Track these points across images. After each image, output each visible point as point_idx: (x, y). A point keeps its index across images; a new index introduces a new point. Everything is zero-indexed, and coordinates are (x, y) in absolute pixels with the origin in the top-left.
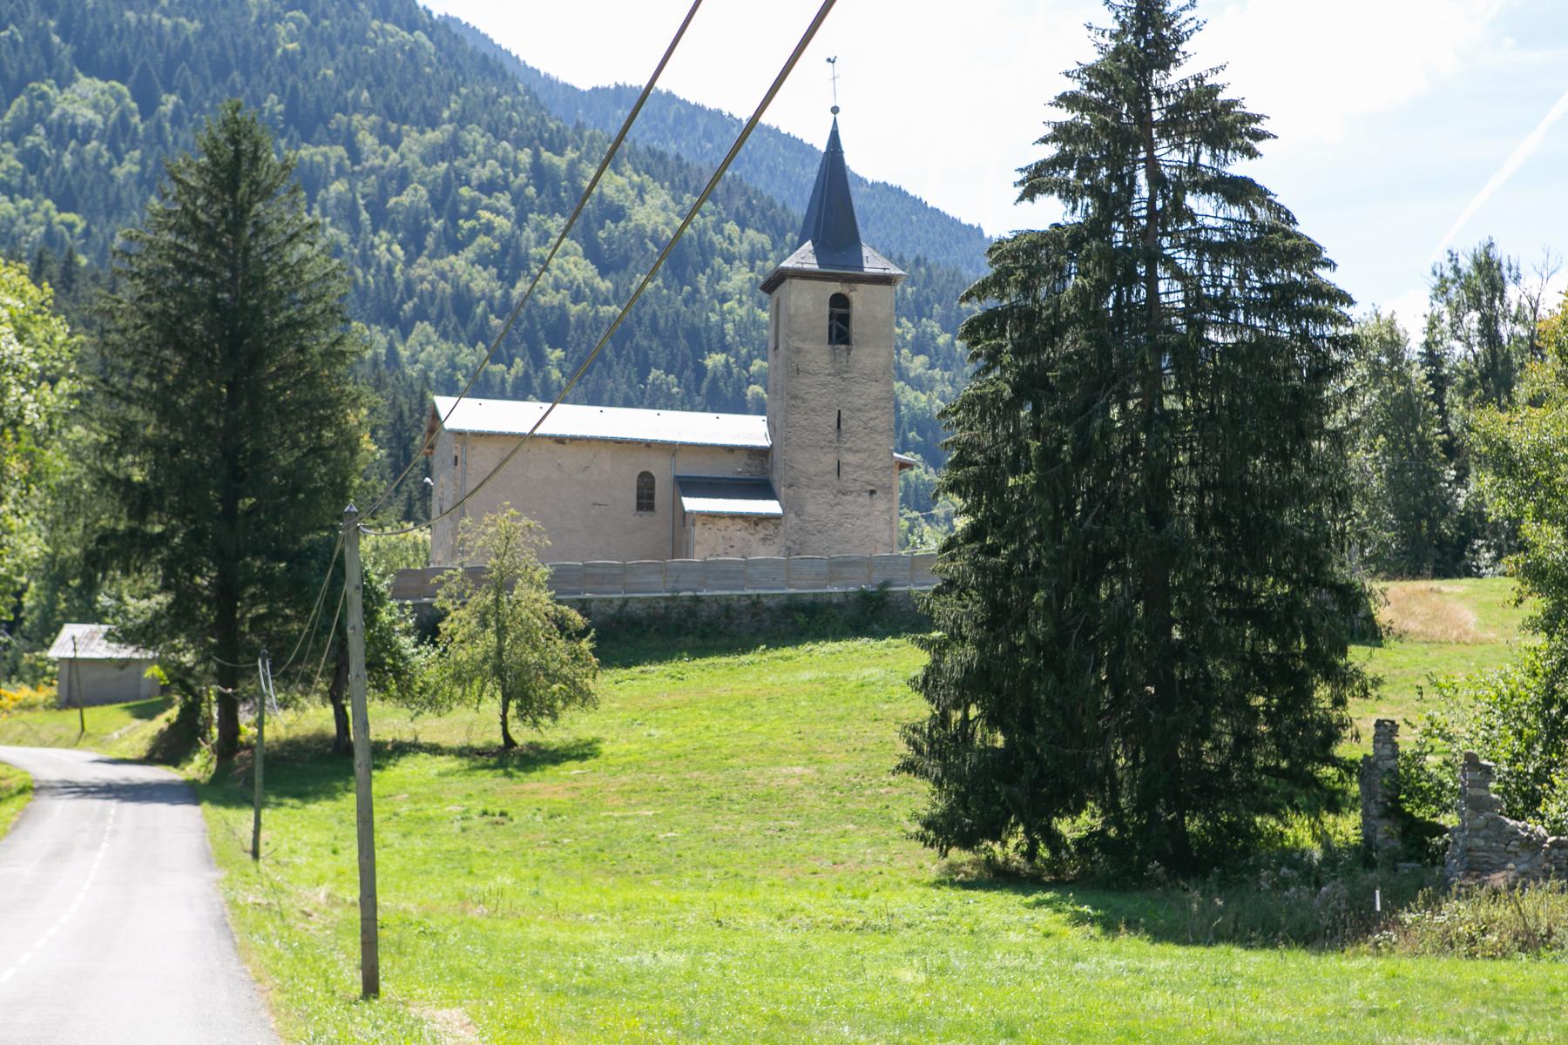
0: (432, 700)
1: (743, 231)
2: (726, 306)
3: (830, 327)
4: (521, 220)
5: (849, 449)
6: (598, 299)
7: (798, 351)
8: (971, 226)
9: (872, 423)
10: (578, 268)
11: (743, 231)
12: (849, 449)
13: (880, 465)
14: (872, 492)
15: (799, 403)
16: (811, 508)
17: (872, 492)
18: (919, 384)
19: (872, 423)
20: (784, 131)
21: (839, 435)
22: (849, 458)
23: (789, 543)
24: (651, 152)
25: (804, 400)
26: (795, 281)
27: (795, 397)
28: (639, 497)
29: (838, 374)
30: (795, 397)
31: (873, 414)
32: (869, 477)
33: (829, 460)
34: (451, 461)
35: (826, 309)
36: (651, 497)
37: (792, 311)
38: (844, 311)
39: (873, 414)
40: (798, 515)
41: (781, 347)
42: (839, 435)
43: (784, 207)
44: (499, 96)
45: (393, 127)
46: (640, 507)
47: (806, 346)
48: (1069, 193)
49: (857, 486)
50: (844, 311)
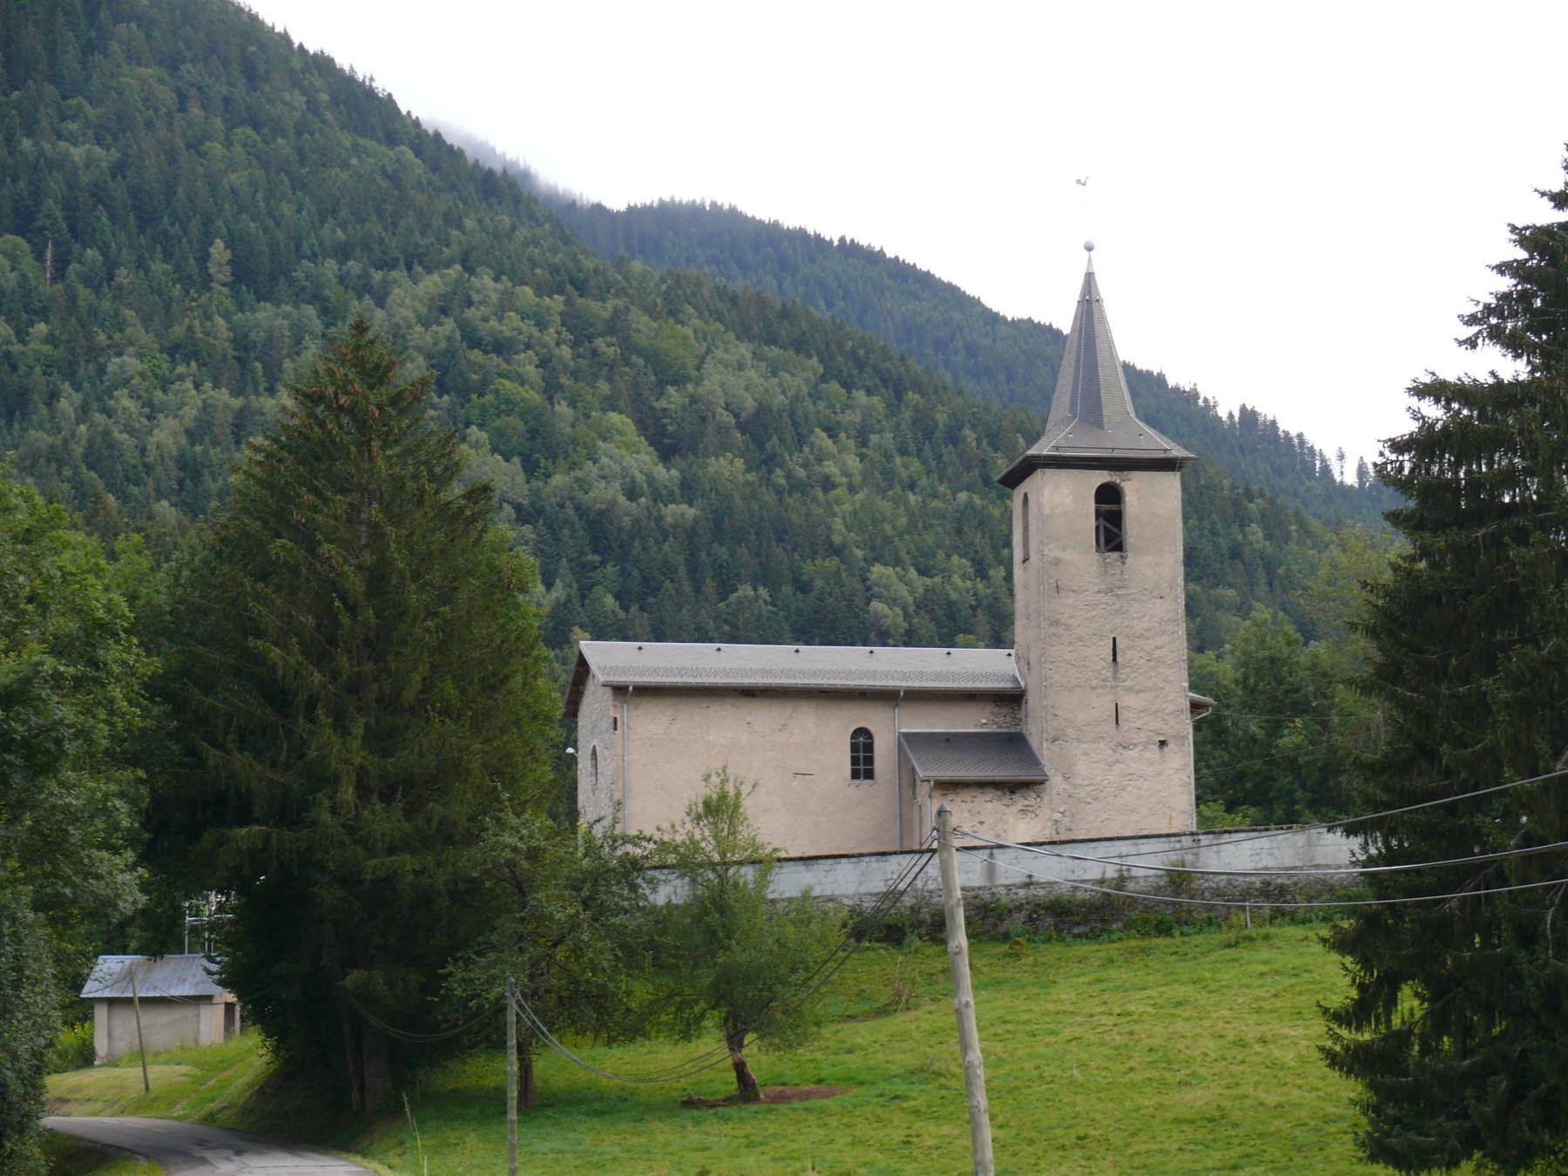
0: (632, 1029)
1: (849, 392)
2: (833, 493)
3: (1097, 528)
4: (551, 390)
5: (1130, 689)
6: (660, 496)
7: (1057, 562)
8: (1149, 373)
9: (1158, 653)
10: (642, 460)
11: (849, 392)
12: (1130, 689)
13: (1171, 708)
14: (1163, 743)
15: (1061, 630)
16: (1082, 768)
17: (1163, 743)
18: (27, 499)
19: (1158, 653)
20: (890, 254)
21: (1116, 671)
22: (1128, 700)
23: (1057, 816)
24: (721, 293)
25: (1068, 627)
26: (1049, 472)
27: (1055, 623)
28: (855, 761)
29: (1110, 590)
30: (1055, 623)
31: (1158, 641)
32: (1158, 725)
33: (1104, 704)
34: (606, 724)
35: (1091, 506)
36: (870, 760)
37: (1047, 510)
38: (1114, 507)
39: (1158, 641)
40: (1066, 778)
41: (1033, 557)
42: (1116, 671)
43: (902, 359)
44: (514, 228)
45: (377, 276)
46: (855, 775)
47: (1067, 556)
48: (1514, 345)
49: (1143, 737)
50: (1114, 507)
